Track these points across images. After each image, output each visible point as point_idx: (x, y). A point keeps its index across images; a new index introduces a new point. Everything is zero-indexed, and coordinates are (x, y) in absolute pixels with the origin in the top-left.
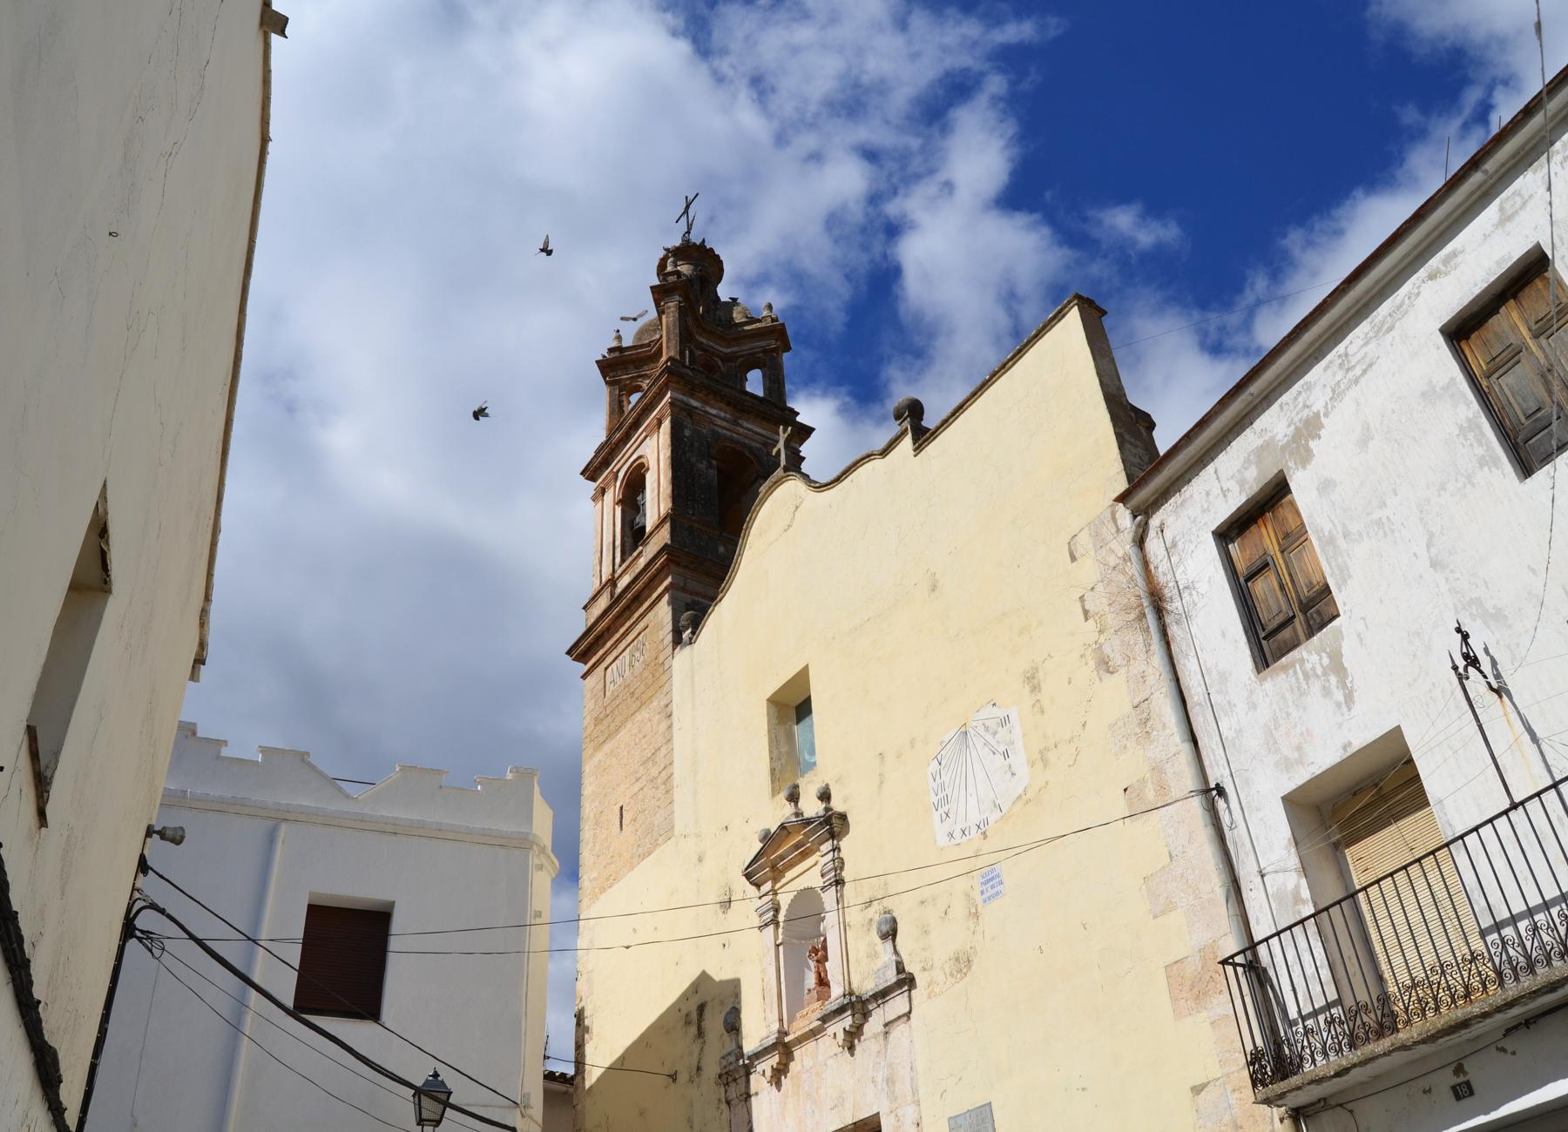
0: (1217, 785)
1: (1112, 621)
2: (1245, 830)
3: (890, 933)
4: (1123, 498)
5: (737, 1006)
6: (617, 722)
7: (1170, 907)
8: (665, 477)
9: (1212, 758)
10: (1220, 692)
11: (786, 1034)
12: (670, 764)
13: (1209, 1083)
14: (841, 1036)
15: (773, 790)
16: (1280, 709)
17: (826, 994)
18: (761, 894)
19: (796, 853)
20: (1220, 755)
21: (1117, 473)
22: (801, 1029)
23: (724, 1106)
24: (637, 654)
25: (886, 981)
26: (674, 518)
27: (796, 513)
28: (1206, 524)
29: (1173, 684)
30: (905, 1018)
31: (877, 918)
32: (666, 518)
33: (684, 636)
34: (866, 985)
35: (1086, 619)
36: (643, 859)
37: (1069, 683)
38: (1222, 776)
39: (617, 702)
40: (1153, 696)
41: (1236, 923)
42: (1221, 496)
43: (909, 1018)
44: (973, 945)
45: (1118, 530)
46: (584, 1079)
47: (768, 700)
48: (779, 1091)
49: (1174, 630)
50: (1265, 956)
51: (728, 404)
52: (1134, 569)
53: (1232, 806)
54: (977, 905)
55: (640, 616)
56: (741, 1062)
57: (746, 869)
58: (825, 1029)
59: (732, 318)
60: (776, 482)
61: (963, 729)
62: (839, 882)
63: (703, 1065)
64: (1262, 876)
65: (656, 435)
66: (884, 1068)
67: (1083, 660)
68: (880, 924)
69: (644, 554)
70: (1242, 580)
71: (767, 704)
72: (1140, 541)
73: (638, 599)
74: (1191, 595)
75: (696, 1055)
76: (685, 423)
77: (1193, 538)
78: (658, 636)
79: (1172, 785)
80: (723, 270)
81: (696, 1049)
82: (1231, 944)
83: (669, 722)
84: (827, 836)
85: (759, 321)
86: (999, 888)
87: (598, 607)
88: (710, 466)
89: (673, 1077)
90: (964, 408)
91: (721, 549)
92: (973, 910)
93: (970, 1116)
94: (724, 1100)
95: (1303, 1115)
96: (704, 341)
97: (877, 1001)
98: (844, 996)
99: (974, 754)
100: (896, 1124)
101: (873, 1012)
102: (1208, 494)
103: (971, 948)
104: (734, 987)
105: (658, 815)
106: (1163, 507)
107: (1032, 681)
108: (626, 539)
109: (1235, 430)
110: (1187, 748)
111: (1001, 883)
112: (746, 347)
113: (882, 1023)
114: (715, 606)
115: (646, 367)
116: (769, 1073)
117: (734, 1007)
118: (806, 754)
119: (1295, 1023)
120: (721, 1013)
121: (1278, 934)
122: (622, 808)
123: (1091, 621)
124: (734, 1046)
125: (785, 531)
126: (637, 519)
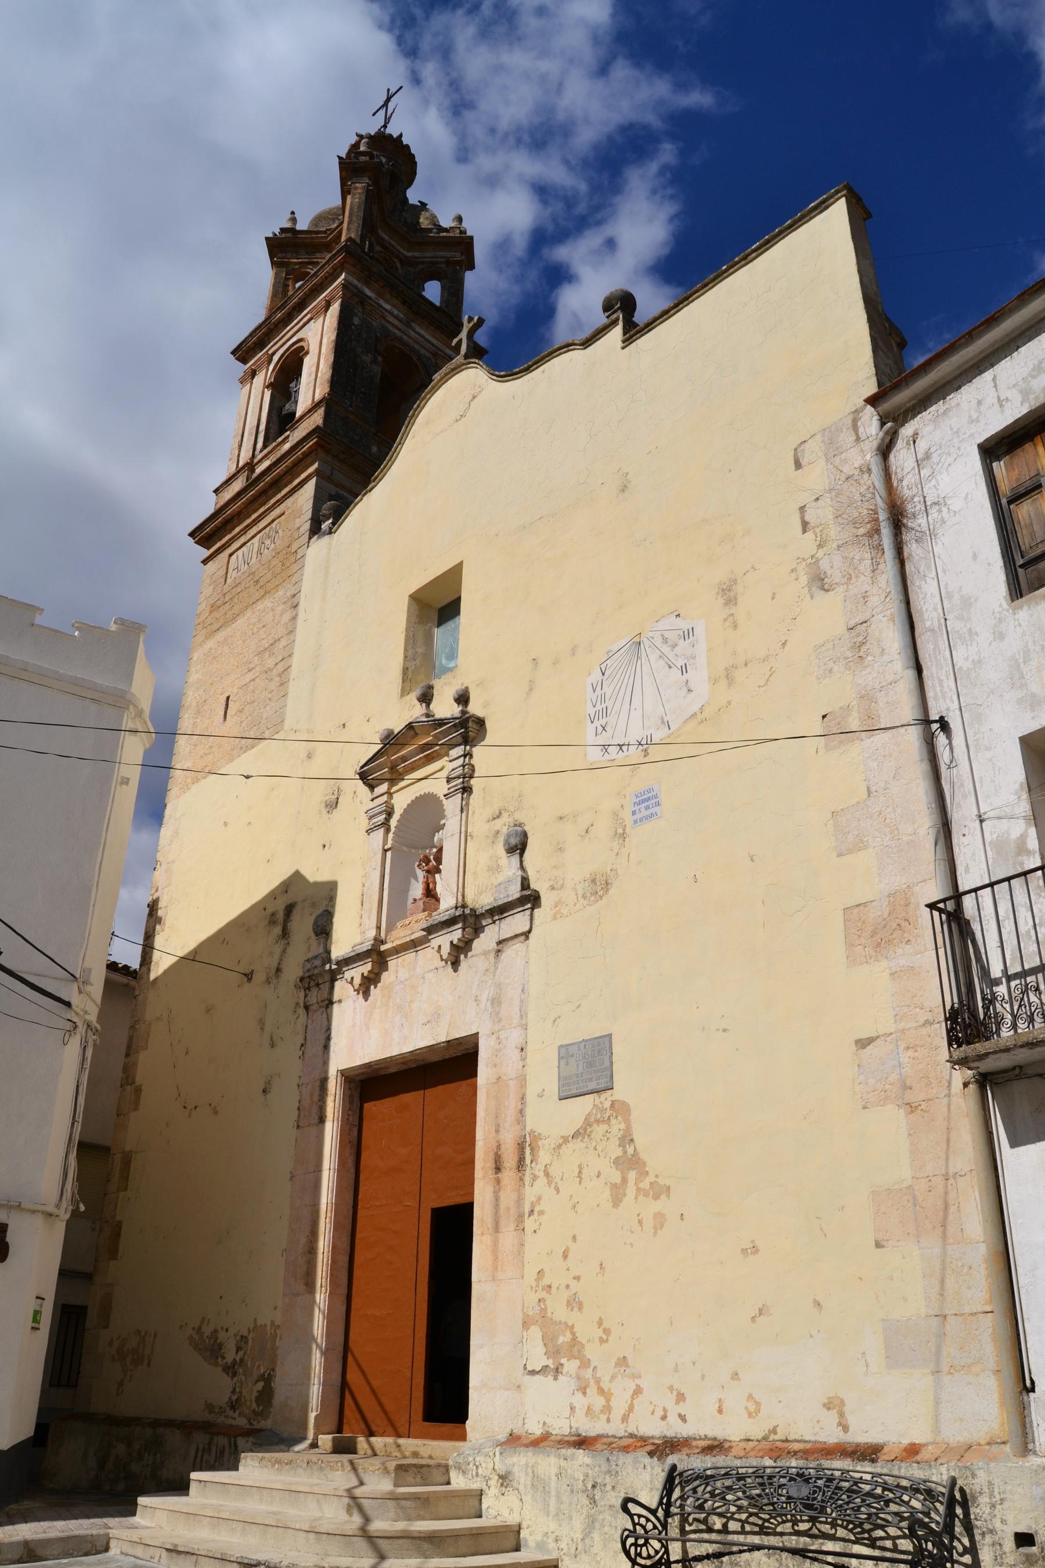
0: (942, 718)
1: (833, 532)
2: (969, 770)
3: (518, 847)
4: (873, 401)
5: (330, 909)
6: (236, 610)
7: (860, 845)
8: (326, 360)
9: (938, 689)
10: (960, 618)
11: (383, 942)
12: (290, 656)
13: (878, 1037)
14: (446, 950)
15: (403, 689)
16: (1034, 642)
17: (433, 906)
18: (375, 796)
19: (421, 756)
20: (948, 686)
21: (868, 378)
22: (399, 939)
23: (301, 1011)
24: (268, 542)
25: (508, 896)
26: (330, 403)
27: (472, 403)
28: (971, 435)
29: (903, 605)
30: (523, 937)
31: (505, 830)
32: (321, 402)
33: (323, 527)
34: (482, 899)
35: (804, 531)
36: (245, 752)
37: (773, 598)
38: (948, 709)
39: (239, 589)
40: (875, 618)
41: (942, 868)
42: (997, 406)
43: (527, 938)
44: (615, 867)
45: (858, 439)
46: (149, 970)
47: (410, 596)
48: (366, 1000)
49: (912, 549)
50: (970, 908)
51: (404, 302)
52: (876, 478)
53: (954, 743)
54: (625, 825)
55: (278, 501)
56: (327, 967)
57: (362, 767)
58: (429, 941)
59: (418, 223)
60: (453, 370)
61: (637, 639)
62: (467, 790)
63: (283, 966)
64: (981, 821)
65: (321, 319)
66: (490, 987)
67: (794, 575)
68: (509, 836)
69: (290, 438)
70: (1004, 501)
71: (409, 600)
72: (885, 450)
73: (277, 485)
74: (940, 511)
75: (277, 956)
76: (356, 311)
77: (952, 450)
78: (294, 524)
79: (882, 716)
80: (415, 173)
81: (278, 950)
82: (935, 891)
83: (295, 613)
84: (460, 740)
85: (446, 230)
86: (657, 809)
87: (231, 491)
88: (375, 361)
89: (249, 976)
90: (690, 299)
91: (374, 449)
92: (620, 831)
93: (585, 1046)
94: (302, 1005)
95: (991, 1081)
96: (387, 238)
97: (493, 916)
98: (456, 908)
99: (646, 668)
100: (497, 1047)
101: (486, 929)
102: (979, 403)
103: (611, 870)
104: (329, 890)
105: (268, 708)
106: (920, 415)
107: (728, 593)
108: (271, 425)
109: (1027, 334)
110: (911, 674)
111: (658, 804)
112: (429, 254)
113: (496, 939)
114: (364, 495)
115: (318, 255)
116: (357, 981)
117: (326, 911)
118: (443, 658)
119: (997, 982)
120: (311, 915)
121: (991, 885)
122: (228, 698)
123: (810, 535)
124: (321, 950)
125: (457, 421)
126: (287, 406)
